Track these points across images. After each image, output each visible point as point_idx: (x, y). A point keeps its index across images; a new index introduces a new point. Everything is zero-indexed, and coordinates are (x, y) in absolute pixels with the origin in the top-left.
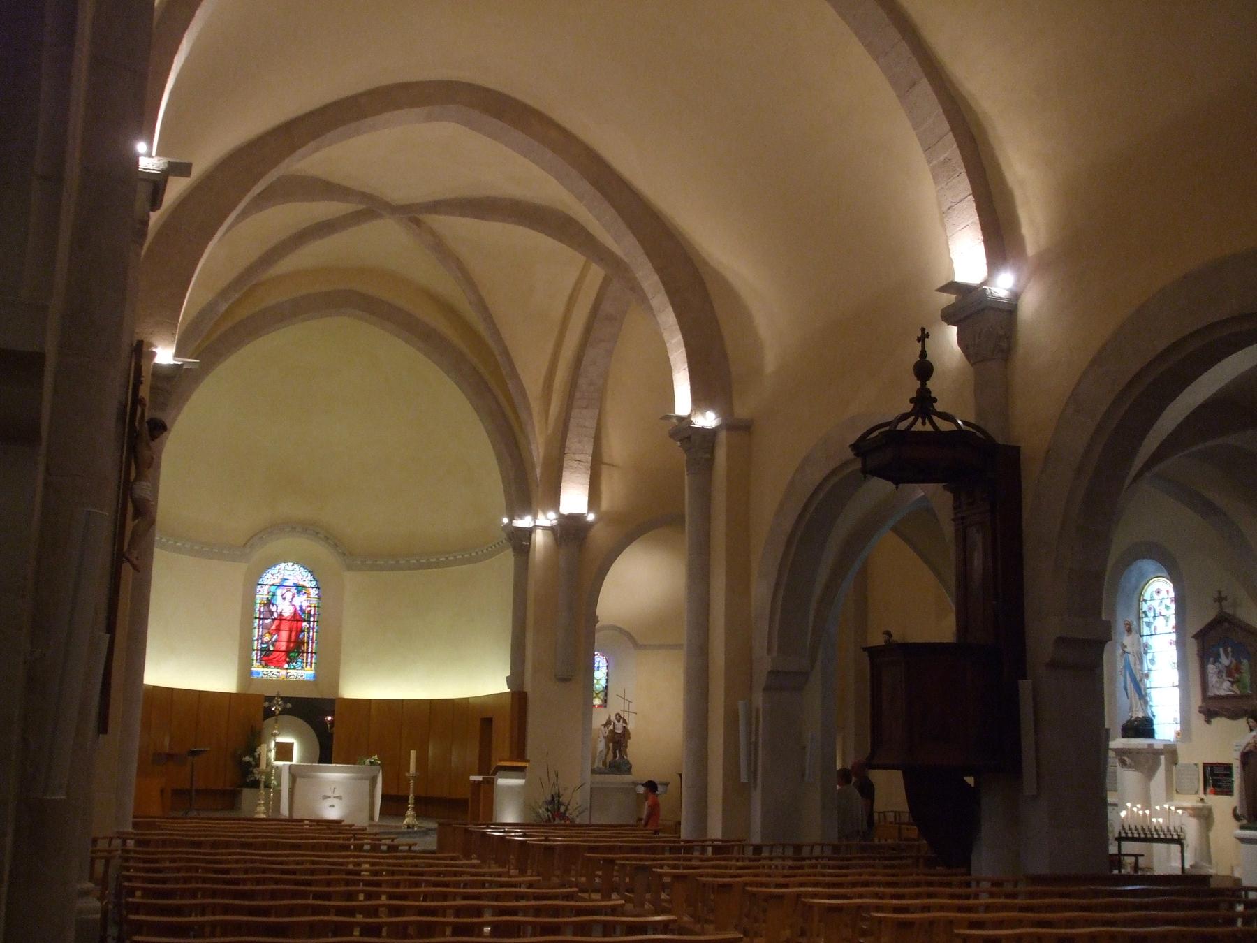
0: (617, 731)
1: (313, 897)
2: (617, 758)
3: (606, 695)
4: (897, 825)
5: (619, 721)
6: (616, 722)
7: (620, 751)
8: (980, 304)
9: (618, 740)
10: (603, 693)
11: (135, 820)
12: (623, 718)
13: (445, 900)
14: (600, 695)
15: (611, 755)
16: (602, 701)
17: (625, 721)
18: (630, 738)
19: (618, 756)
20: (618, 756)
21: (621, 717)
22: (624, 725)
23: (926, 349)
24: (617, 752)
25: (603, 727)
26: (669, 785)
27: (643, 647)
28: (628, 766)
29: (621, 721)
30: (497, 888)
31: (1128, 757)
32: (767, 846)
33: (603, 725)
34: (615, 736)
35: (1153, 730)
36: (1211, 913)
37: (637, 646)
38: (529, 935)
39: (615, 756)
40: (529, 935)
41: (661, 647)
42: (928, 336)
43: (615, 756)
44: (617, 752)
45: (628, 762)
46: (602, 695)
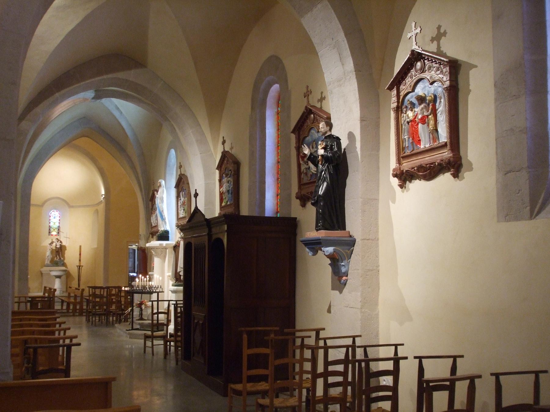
1: (13, 331)
4: (151, 302)
6: (57, 242)
7: (59, 256)
8: (529, 172)
9: (60, 251)
10: (57, 229)
11: (270, 340)
13: (33, 335)
17: (61, 242)
22: (60, 244)
23: (322, 106)
25: (49, 245)
27: (72, 207)
29: (59, 242)
30: (39, 327)
31: (153, 251)
32: (66, 302)
33: (49, 244)
35: (169, 236)
36: (15, 323)
37: (70, 206)
41: (80, 206)
42: (324, 98)
46: (56, 230)
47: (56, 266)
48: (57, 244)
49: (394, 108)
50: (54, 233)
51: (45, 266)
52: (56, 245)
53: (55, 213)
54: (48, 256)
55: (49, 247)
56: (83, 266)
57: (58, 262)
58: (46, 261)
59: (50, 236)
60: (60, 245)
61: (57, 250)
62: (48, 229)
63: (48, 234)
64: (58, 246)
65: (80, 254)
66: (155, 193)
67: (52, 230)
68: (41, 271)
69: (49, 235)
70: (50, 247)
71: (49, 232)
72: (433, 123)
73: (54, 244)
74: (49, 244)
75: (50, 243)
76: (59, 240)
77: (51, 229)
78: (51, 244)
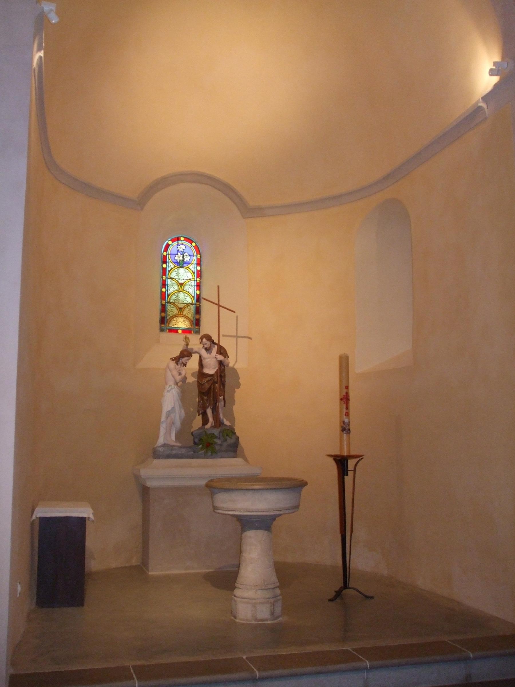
0: (206, 371)
2: (208, 426)
3: (198, 311)
5: (208, 350)
6: (204, 352)
7: (215, 410)
10: (192, 308)
12: (218, 345)
14: (185, 312)
15: (198, 421)
16: (191, 322)
17: (222, 351)
18: (238, 386)
19: (211, 419)
20: (211, 419)
21: (213, 342)
22: (220, 358)
24: (209, 411)
25: (173, 364)
26: (305, 489)
28: (230, 441)
29: (215, 349)
33: (172, 359)
34: (204, 381)
38: (345, 475)
39: (205, 421)
40: (345, 475)
43: (205, 421)
44: (209, 411)
45: (231, 432)
46: (190, 312)
47: (206, 456)
48: (205, 362)
49: (349, 425)
50: (181, 323)
51: (156, 455)
52: (201, 365)
53: (182, 248)
54: (169, 413)
55: (175, 373)
56: (359, 457)
57: (213, 436)
58: (162, 431)
59: (166, 336)
60: (221, 363)
61: (207, 386)
62: (159, 307)
63: (158, 328)
64: (211, 370)
65: (345, 399)
66: (213, 424)
67: (172, 310)
68: (137, 477)
69: (162, 330)
70: (180, 374)
71: (163, 320)
72: (19, 588)
73: (193, 364)
74: (172, 359)
75: (177, 354)
76: (215, 344)
77: (169, 306)
78: (184, 360)
